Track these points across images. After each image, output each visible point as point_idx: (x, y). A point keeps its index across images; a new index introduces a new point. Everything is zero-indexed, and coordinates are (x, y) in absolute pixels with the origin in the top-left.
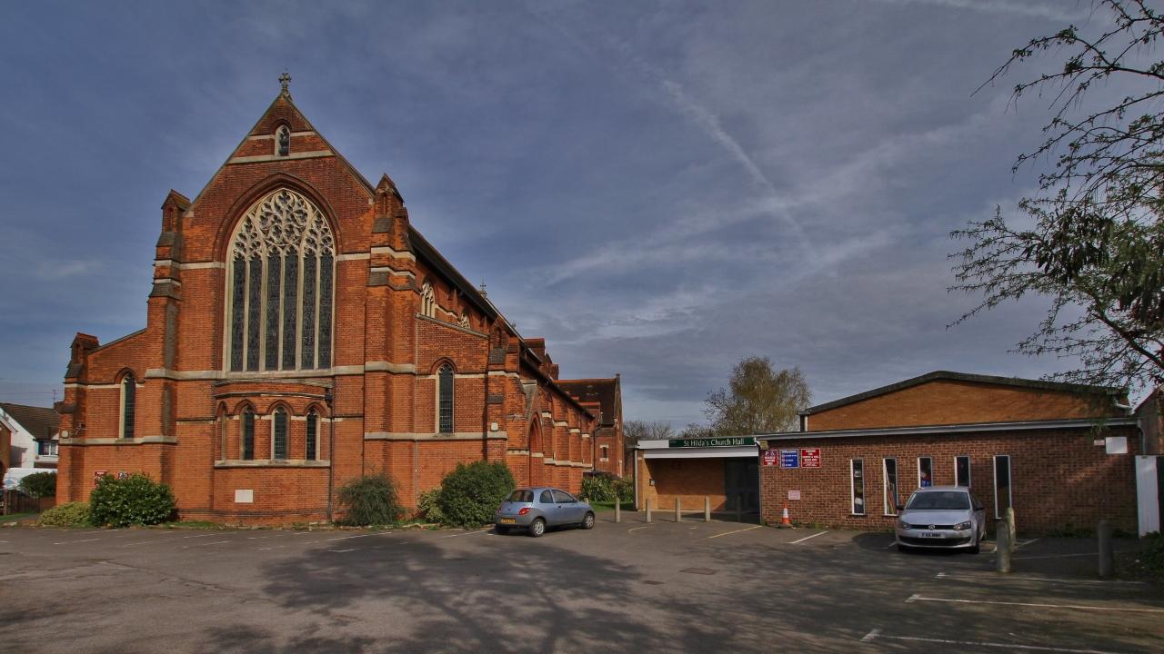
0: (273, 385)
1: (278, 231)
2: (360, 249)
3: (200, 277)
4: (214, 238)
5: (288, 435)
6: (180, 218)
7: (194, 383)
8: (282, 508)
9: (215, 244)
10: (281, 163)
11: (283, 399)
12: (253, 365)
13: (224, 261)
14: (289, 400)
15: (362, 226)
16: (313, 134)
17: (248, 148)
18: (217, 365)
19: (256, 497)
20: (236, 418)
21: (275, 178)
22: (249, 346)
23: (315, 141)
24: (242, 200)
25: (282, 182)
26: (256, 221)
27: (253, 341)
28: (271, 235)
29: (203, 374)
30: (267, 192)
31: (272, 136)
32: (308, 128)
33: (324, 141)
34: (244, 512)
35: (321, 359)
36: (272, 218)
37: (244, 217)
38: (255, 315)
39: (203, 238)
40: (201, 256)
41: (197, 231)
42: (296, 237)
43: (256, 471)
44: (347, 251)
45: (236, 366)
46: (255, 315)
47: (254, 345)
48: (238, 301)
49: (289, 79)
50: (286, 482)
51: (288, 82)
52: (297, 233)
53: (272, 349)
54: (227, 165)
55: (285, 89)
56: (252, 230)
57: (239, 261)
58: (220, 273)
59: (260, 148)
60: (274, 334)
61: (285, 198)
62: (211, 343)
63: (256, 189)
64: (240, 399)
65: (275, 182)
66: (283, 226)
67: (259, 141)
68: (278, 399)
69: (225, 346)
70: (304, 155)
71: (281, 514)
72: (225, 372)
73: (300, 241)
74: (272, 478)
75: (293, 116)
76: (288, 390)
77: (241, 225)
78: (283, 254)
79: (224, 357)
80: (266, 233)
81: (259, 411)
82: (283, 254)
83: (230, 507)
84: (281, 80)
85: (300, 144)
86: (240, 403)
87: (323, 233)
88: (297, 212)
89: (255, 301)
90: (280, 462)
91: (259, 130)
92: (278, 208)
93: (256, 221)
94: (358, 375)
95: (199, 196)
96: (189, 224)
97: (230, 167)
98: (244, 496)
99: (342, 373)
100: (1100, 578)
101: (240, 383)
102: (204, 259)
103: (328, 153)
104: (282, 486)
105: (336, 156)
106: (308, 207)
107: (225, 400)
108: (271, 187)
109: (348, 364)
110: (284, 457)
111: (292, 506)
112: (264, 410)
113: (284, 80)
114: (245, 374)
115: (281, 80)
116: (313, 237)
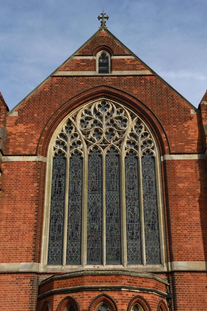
1: (98, 133)
2: (186, 151)
3: (23, 169)
4: (39, 135)
6: (6, 116)
7: (9, 276)
9: (39, 140)
10: (104, 78)
11: (141, 295)
12: (75, 258)
13: (46, 155)
15: (186, 132)
16: (133, 58)
17: (70, 64)
18: (37, 259)
21: (99, 89)
23: (135, 63)
24: (67, 105)
25: (109, 94)
26: (78, 125)
28: (91, 135)
29: (22, 266)
30: (88, 101)
31: (95, 58)
32: (127, 52)
33: (143, 63)
36: (91, 122)
37: (66, 119)
38: (75, 208)
39: (26, 134)
40: (25, 149)
41: (21, 128)
42: (117, 139)
44: (174, 152)
45: (55, 258)
46: (75, 208)
47: (75, 237)
48: (58, 192)
49: (107, 18)
51: (106, 20)
52: (117, 135)
54: (52, 76)
55: (103, 24)
56: (73, 131)
57: (60, 155)
58: (41, 166)
59: (83, 66)
60: (97, 227)
61: (104, 105)
63: (82, 96)
64: (97, 294)
65: (98, 93)
66: (105, 129)
67: (83, 61)
68: (136, 294)
69: (43, 237)
70: (125, 73)
72: (42, 266)
73: (121, 142)
75: (114, 44)
77: (62, 125)
78: (85, 154)
79: (42, 248)
80: (86, 133)
82: (85, 154)
84: (99, 18)
85: (122, 65)
86: (98, 297)
87: (72, 137)
88: (116, 118)
89: (76, 194)
91: (82, 52)
92: (98, 114)
93: (78, 125)
94: (200, 272)
95: (24, 99)
96: (13, 122)
97: (55, 78)
99: (181, 269)
101: (94, 274)
102: (27, 153)
103: (148, 72)
105: (154, 74)
106: (127, 113)
107: (74, 295)
108: (93, 97)
109: (187, 259)
113: (103, 18)
114: (67, 268)
115: (99, 18)
116: (62, 139)
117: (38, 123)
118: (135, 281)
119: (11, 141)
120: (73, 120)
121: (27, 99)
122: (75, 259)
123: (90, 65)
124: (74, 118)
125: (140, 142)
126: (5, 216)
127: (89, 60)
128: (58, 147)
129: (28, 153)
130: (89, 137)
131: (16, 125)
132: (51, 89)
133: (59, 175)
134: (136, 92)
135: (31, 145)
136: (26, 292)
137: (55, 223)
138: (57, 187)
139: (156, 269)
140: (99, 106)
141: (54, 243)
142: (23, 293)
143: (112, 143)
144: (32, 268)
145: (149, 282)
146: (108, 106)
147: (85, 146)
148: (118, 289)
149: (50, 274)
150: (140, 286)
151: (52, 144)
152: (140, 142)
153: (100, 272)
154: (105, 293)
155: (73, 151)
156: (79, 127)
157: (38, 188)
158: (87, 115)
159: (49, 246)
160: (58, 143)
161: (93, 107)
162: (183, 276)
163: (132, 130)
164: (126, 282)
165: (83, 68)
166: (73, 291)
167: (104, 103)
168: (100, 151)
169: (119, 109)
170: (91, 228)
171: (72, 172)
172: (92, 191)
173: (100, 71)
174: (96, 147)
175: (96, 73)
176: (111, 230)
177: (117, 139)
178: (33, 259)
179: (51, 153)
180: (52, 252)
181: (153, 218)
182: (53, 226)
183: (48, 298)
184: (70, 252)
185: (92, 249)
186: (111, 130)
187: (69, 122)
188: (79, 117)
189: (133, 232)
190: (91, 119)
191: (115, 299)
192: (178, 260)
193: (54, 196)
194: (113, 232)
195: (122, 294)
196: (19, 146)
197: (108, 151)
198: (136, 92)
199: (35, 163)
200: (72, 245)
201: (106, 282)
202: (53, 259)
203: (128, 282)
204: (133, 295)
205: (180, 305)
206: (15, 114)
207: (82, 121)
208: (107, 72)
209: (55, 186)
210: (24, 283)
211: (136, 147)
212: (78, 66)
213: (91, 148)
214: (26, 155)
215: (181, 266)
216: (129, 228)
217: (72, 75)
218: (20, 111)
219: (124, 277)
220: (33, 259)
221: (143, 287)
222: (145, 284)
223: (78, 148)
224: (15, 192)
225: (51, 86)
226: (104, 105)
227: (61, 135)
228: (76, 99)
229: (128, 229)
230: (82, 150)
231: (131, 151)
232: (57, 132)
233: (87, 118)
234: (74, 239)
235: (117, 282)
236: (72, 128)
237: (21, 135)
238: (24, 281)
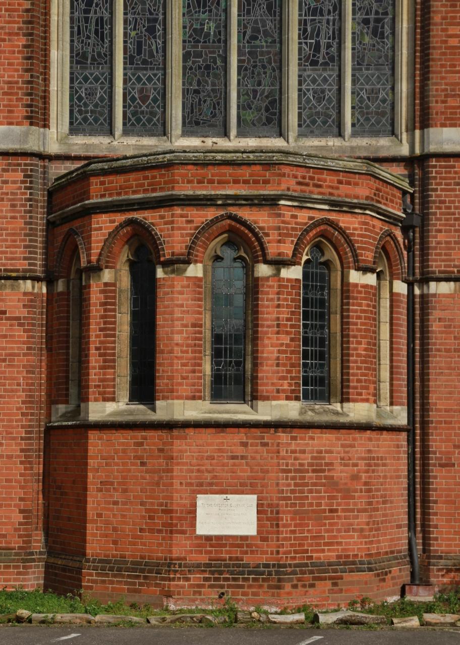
0: (311, 169)
5: (336, 326)
8: (329, 555)
11: (333, 217)
14: (344, 221)
18: (38, 116)
19: (267, 514)
20: (195, 270)
22: (129, 60)
27: (151, 30)
34: (227, 563)
35: (192, 96)
43: (268, 436)
50: (340, 473)
53: (205, 67)
60: (211, 27)
62: (22, 41)
64: (210, 214)
68: (318, 216)
69: (54, 54)
71: (332, 572)
72: (55, 137)
74: (307, 459)
76: (344, 192)
81: (272, 250)
83: (180, 548)
90: (319, 411)
94: (44, 144)
98: (228, 516)
100: (251, 392)
101: (203, 162)
104: (332, 484)
110: (326, 397)
111: (354, 545)
112: (287, 249)
114: (125, 144)
118: (319, 180)
122: (150, 121)
136: (13, 206)
137: (87, 11)
139: (378, 149)
141: (87, 72)
144: (25, 141)
145: (356, 184)
148: (271, 202)
150: (331, 194)
153: (219, 156)
154: (234, 211)
159: (72, 80)
162: (454, 167)
164: (292, 183)
166: (144, 205)
170: (195, 30)
176: (254, 38)
180: (80, 99)
182: (82, 24)
184: (133, 99)
185: (197, 92)
189: (318, 44)
191: (261, 228)
192: (443, 125)
194: (258, 42)
195: (279, 215)
200: (139, 79)
201: (236, 182)
202: (85, 119)
203: (299, 183)
204: (311, 218)
205: (438, 243)
215: (449, 141)
216: (305, 30)
219: (286, 170)
220: (27, 118)
221: (339, 196)
222: (344, 189)
229: (303, 33)
234: (145, 62)
235: (266, 182)
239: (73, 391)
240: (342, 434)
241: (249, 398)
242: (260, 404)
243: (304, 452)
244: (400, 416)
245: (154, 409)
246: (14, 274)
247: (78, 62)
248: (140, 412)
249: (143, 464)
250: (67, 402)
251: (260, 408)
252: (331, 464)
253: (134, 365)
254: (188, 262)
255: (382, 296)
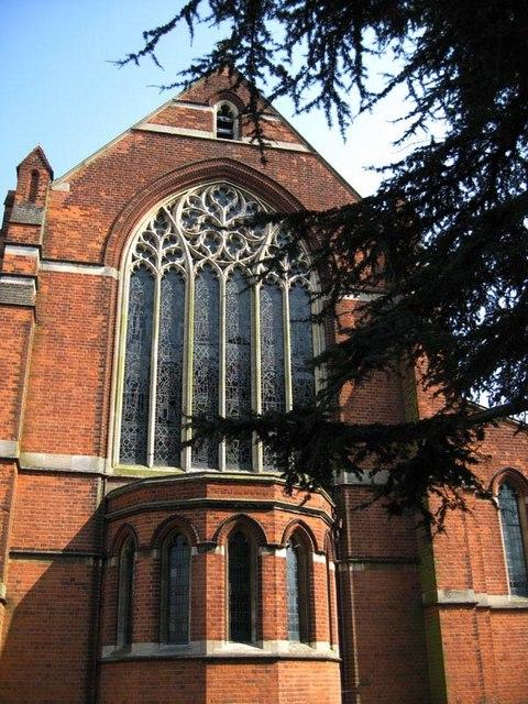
1: (213, 241)
18: (101, 449)
24: (160, 183)
28: (201, 241)
29: (79, 462)
39: (83, 226)
41: (75, 213)
56: (168, 232)
58: (107, 288)
67: (191, 112)
72: (112, 464)
102: (85, 260)
103: (302, 148)
105: (313, 153)
114: (156, 469)
117: (107, 209)
119: (55, 234)
120: (168, 212)
121: (88, 163)
123: (203, 120)
124: (172, 208)
125: (161, 252)
126: (42, 370)
127: (201, 112)
128: (140, 257)
129: (88, 261)
130: (198, 245)
131: (66, 207)
132: (132, 152)
133: (143, 309)
134: (284, 177)
135: (94, 245)
138: (137, 328)
140: (216, 194)
142: (78, 508)
143: (238, 261)
146: (231, 196)
147: (191, 259)
149: (125, 479)
151: (131, 249)
152: (161, 252)
155: (167, 266)
156: (179, 225)
157: (105, 324)
158: (193, 206)
160: (139, 249)
161: (204, 195)
163: (148, 228)
165: (190, 123)
166: (183, 507)
167: (224, 189)
168: (215, 272)
169: (250, 204)
171: (166, 304)
172: (202, 339)
173: (219, 135)
174: (208, 264)
175: (213, 136)
177: (245, 255)
178: (95, 451)
179: (129, 266)
180: (127, 442)
181: (307, 395)
182: (130, 397)
183: (188, 514)
184: (160, 444)
186: (236, 238)
187: (162, 214)
188: (180, 210)
190: (201, 213)
193: (131, 342)
196: (70, 245)
197: (230, 274)
198: (284, 177)
199: (100, 280)
206: (66, 188)
207: (184, 216)
208: (231, 137)
209: (135, 326)
210: (78, 492)
211: (154, 259)
212: (181, 120)
213: (201, 263)
214: (84, 264)
217: (173, 133)
218: (76, 183)
220: (95, 451)
223: (176, 263)
224: (63, 327)
225: (133, 147)
226: (224, 194)
227: (147, 236)
228: (176, 175)
230: (183, 266)
231: (143, 265)
232: (140, 229)
233: (193, 212)
236: (165, 226)
237: (75, 226)
238: (82, 488)
239: (121, 635)
240: (313, 664)
241: (254, 639)
242: (265, 643)
243: (292, 677)
244: (336, 655)
245: (262, 648)
246: (82, 553)
247: (126, 420)
248: (302, 649)
249: (182, 687)
250: (115, 644)
251: (265, 646)
252: (307, 685)
253: (232, 608)
254: (216, 546)
255: (84, 595)
